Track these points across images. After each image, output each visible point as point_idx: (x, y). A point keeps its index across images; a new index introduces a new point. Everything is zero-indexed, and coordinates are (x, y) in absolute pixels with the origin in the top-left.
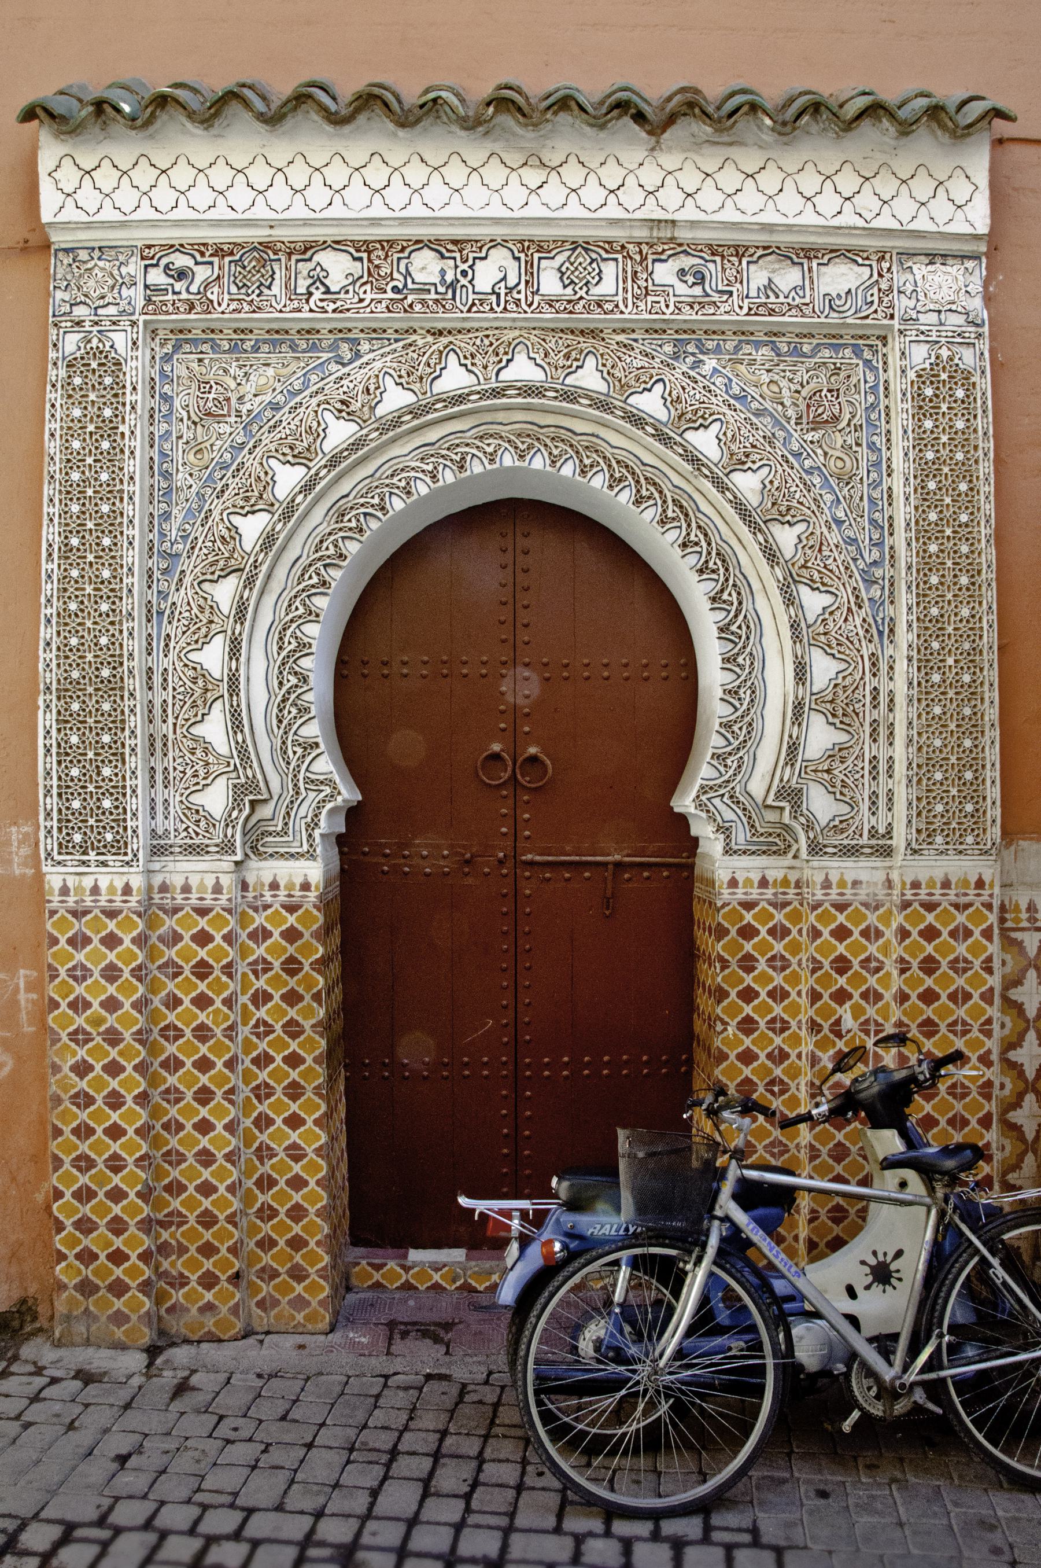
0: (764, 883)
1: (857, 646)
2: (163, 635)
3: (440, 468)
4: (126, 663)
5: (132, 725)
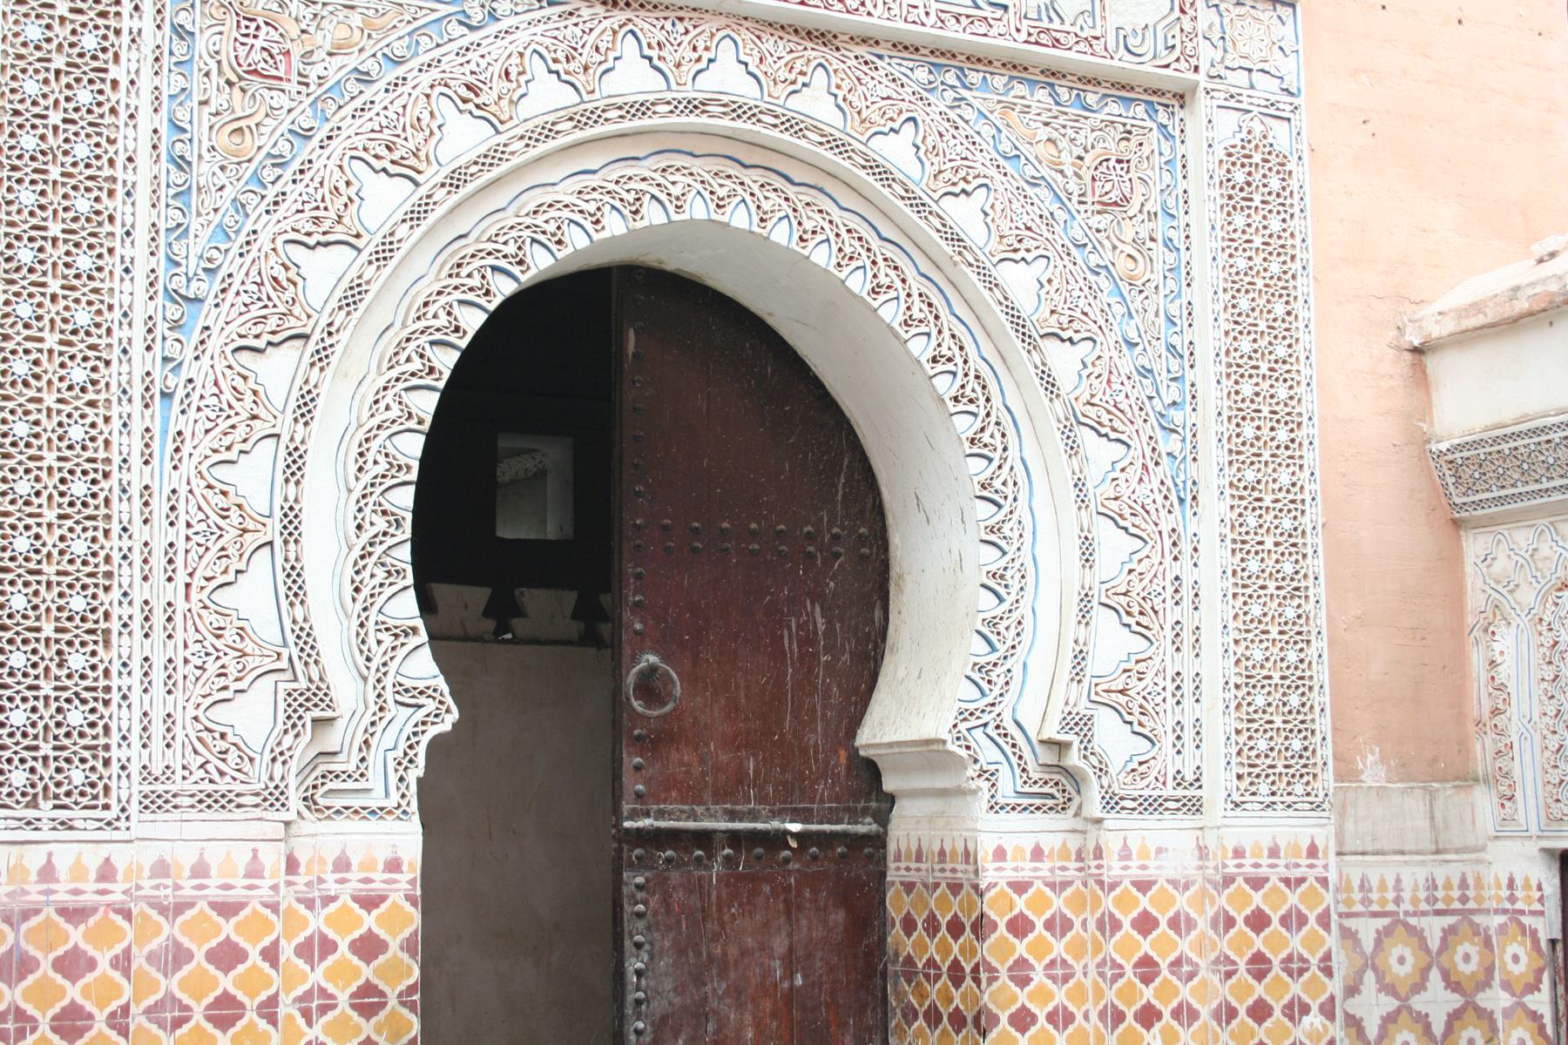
0: (1037, 854)
1: (1154, 517)
2: (172, 431)
3: (607, 209)
4: (115, 475)
5: (125, 582)
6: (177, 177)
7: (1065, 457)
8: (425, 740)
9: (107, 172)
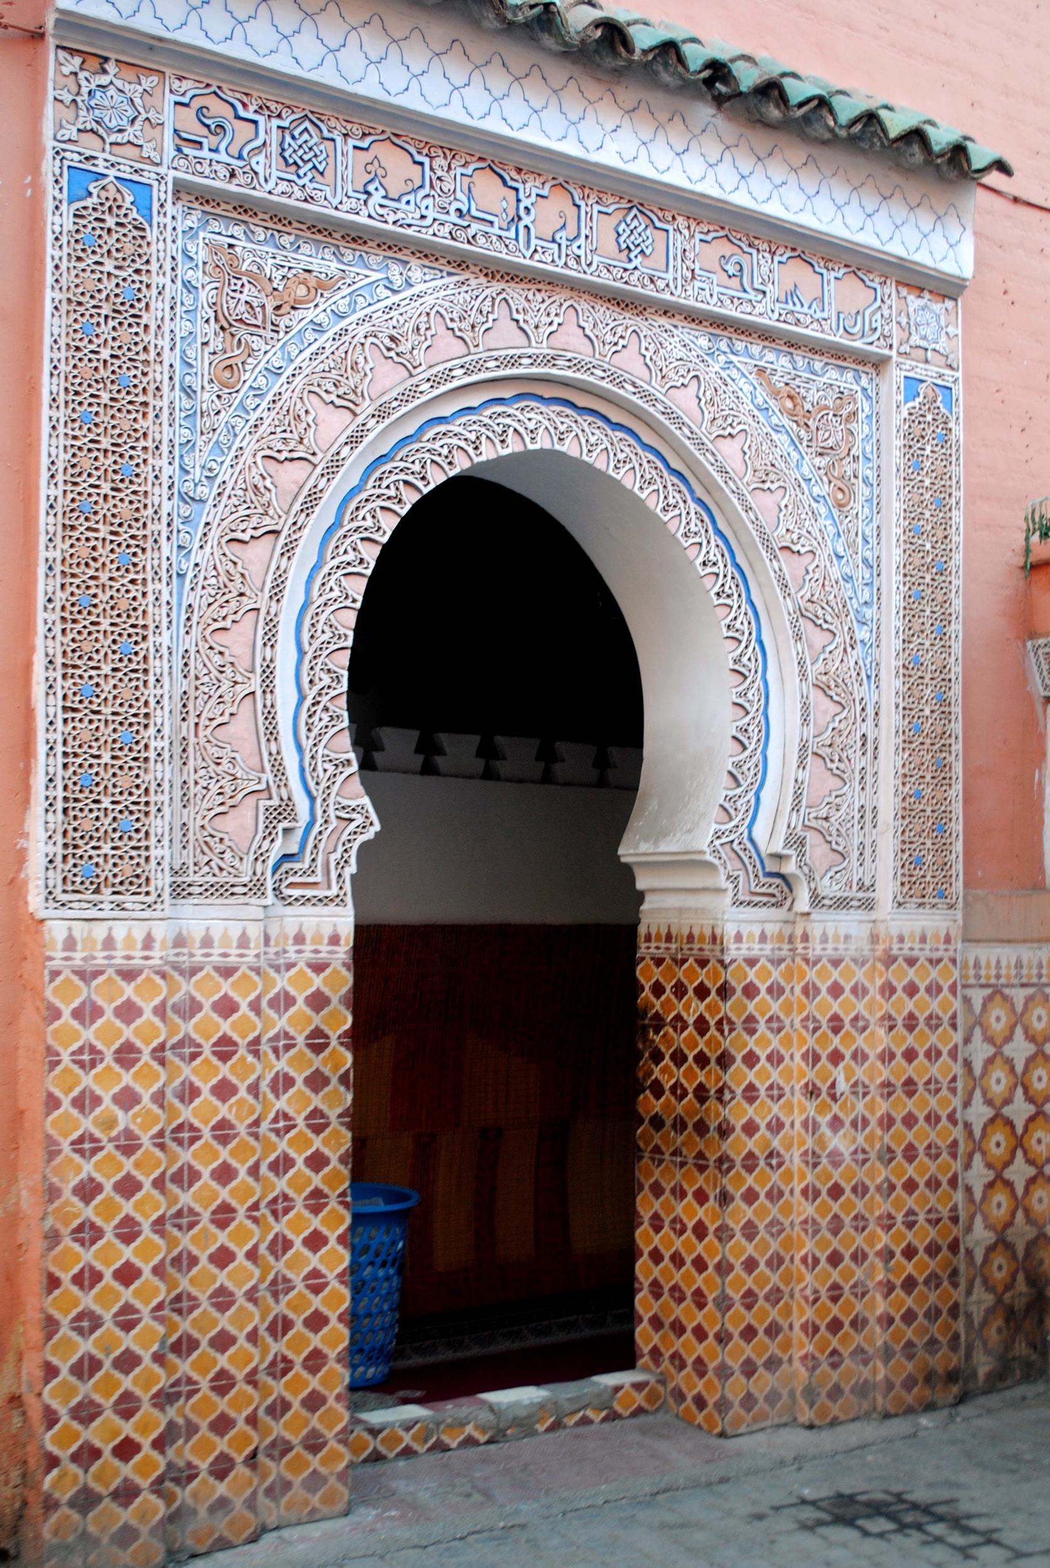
0: (763, 938)
3: (483, 438)
4: (151, 638)
6: (186, 403)
8: (356, 846)
9: (141, 399)
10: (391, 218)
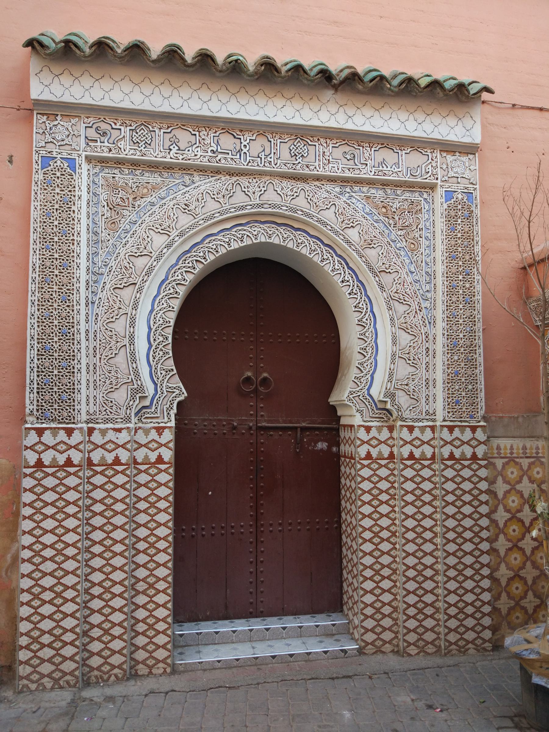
3: (232, 240)
4: (76, 327)
6: (95, 238)
7: (387, 311)
10: (181, 157)
